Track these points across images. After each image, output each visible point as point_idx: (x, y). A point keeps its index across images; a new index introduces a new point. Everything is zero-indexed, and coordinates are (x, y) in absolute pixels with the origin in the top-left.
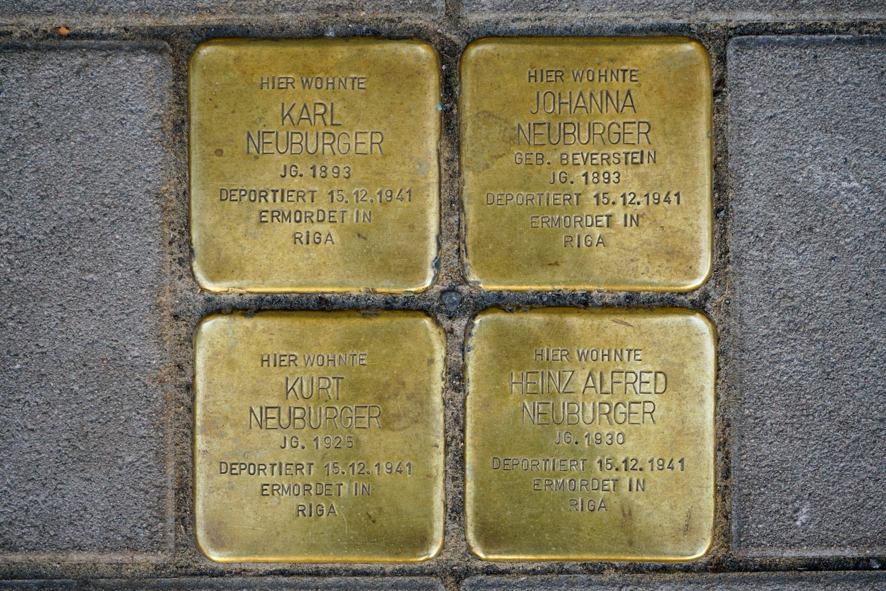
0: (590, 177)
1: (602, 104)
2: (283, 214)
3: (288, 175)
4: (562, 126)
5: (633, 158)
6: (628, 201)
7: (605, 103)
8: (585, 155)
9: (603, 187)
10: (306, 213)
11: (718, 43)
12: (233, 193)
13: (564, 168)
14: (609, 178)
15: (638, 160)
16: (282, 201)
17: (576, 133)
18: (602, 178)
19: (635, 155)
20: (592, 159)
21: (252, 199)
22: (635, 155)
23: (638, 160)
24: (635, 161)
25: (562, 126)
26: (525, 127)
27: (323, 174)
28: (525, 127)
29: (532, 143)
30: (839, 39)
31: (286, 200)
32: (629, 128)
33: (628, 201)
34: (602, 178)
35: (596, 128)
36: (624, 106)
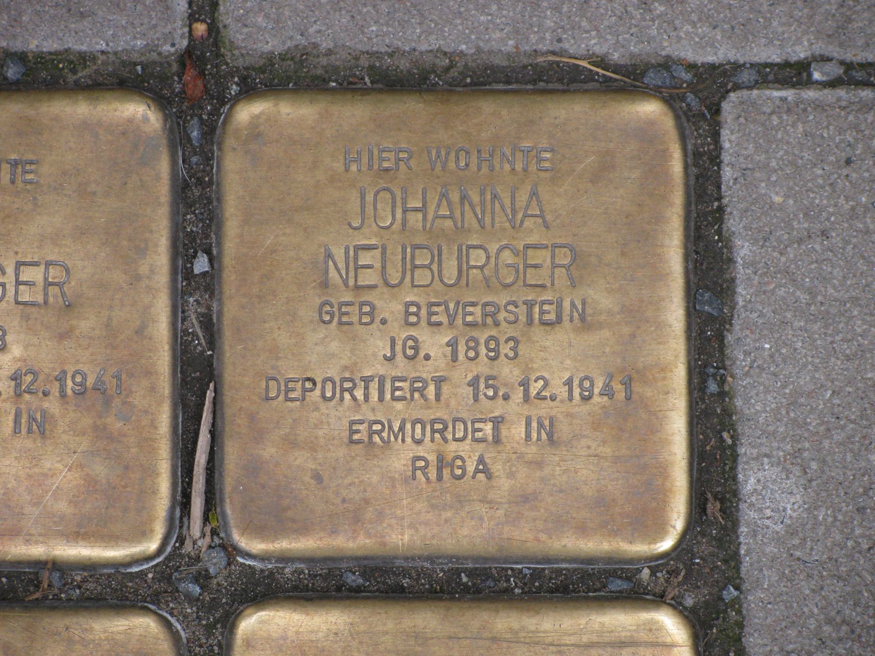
0: (462, 348)
1: (483, 212)
2: (390, 428)
3: (399, 357)
4: (352, 253)
5: (542, 312)
6: (533, 392)
7: (488, 210)
8: (452, 306)
9: (482, 367)
10: (473, 423)
11: (700, 96)
12: (291, 385)
13: (413, 332)
14: (497, 350)
15: (552, 317)
16: (381, 399)
17: (435, 267)
18: (483, 351)
19: (546, 307)
20: (465, 315)
21: (329, 394)
22: (546, 307)
23: (552, 317)
24: (547, 317)
25: (352, 253)
26: (339, 253)
27: (472, 354)
28: (339, 253)
29: (351, 282)
30: (535, 84)
31: (388, 396)
32: (535, 257)
33: (533, 392)
34: (483, 351)
35: (472, 257)
36: (525, 216)
